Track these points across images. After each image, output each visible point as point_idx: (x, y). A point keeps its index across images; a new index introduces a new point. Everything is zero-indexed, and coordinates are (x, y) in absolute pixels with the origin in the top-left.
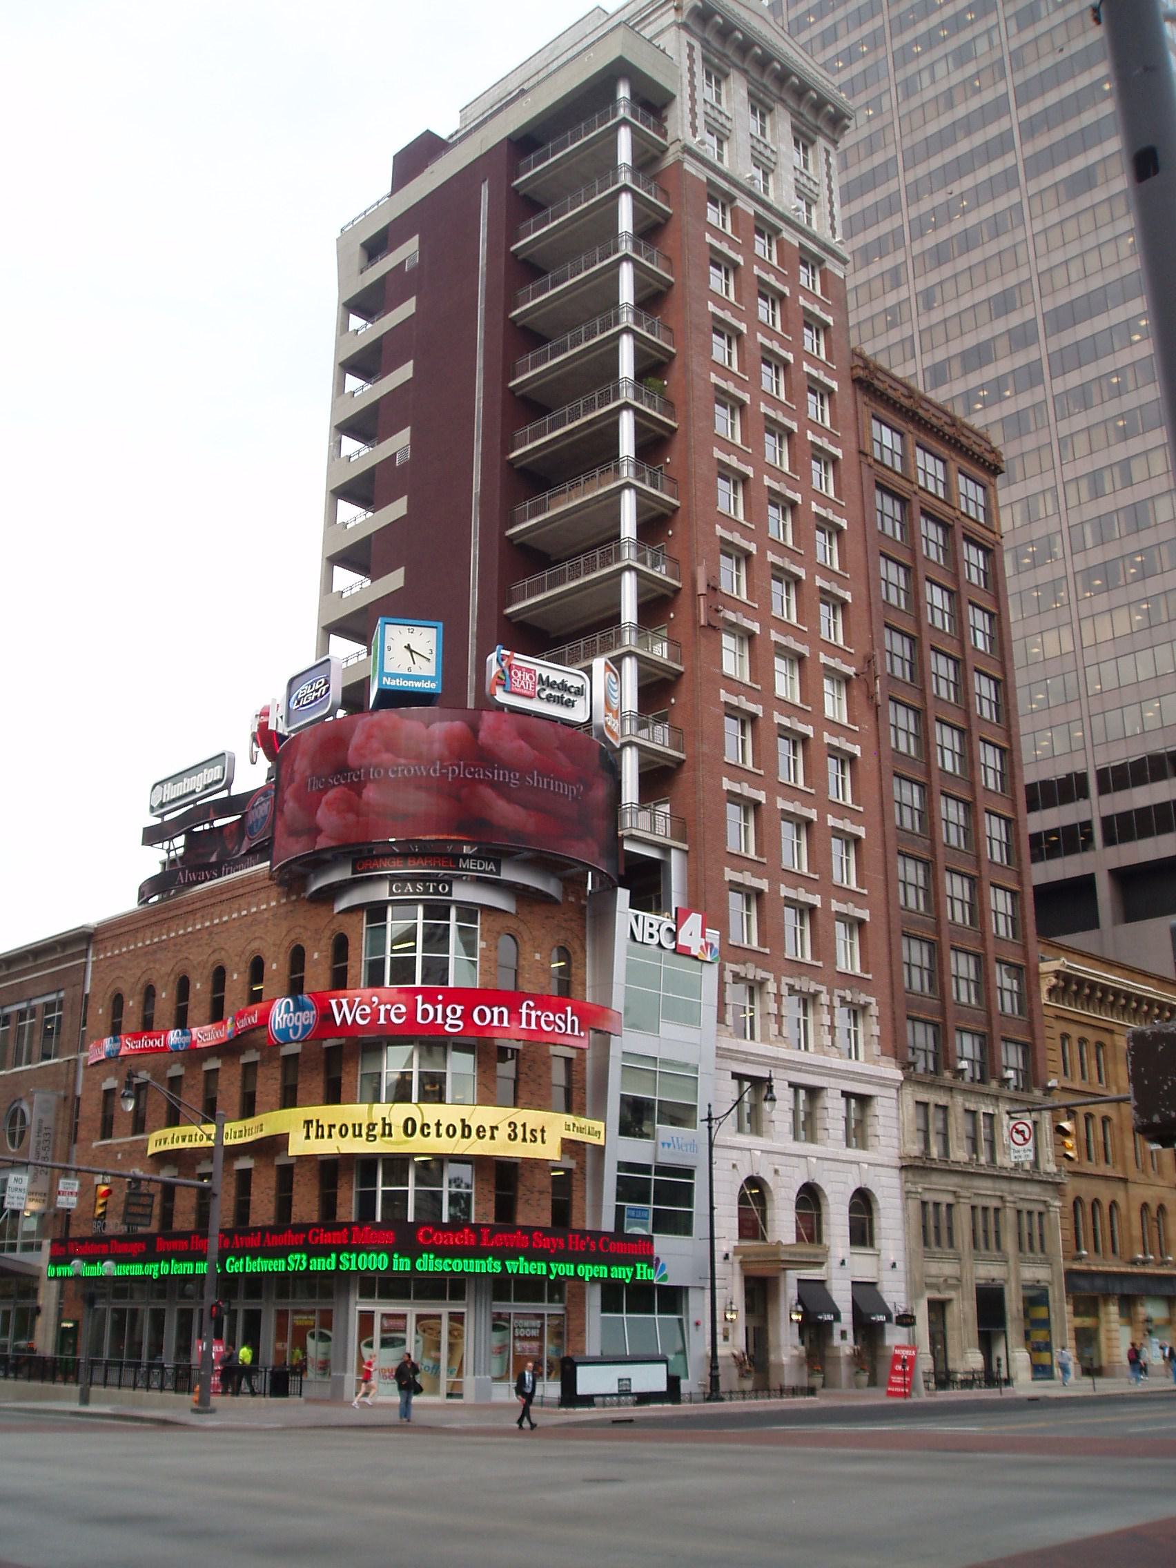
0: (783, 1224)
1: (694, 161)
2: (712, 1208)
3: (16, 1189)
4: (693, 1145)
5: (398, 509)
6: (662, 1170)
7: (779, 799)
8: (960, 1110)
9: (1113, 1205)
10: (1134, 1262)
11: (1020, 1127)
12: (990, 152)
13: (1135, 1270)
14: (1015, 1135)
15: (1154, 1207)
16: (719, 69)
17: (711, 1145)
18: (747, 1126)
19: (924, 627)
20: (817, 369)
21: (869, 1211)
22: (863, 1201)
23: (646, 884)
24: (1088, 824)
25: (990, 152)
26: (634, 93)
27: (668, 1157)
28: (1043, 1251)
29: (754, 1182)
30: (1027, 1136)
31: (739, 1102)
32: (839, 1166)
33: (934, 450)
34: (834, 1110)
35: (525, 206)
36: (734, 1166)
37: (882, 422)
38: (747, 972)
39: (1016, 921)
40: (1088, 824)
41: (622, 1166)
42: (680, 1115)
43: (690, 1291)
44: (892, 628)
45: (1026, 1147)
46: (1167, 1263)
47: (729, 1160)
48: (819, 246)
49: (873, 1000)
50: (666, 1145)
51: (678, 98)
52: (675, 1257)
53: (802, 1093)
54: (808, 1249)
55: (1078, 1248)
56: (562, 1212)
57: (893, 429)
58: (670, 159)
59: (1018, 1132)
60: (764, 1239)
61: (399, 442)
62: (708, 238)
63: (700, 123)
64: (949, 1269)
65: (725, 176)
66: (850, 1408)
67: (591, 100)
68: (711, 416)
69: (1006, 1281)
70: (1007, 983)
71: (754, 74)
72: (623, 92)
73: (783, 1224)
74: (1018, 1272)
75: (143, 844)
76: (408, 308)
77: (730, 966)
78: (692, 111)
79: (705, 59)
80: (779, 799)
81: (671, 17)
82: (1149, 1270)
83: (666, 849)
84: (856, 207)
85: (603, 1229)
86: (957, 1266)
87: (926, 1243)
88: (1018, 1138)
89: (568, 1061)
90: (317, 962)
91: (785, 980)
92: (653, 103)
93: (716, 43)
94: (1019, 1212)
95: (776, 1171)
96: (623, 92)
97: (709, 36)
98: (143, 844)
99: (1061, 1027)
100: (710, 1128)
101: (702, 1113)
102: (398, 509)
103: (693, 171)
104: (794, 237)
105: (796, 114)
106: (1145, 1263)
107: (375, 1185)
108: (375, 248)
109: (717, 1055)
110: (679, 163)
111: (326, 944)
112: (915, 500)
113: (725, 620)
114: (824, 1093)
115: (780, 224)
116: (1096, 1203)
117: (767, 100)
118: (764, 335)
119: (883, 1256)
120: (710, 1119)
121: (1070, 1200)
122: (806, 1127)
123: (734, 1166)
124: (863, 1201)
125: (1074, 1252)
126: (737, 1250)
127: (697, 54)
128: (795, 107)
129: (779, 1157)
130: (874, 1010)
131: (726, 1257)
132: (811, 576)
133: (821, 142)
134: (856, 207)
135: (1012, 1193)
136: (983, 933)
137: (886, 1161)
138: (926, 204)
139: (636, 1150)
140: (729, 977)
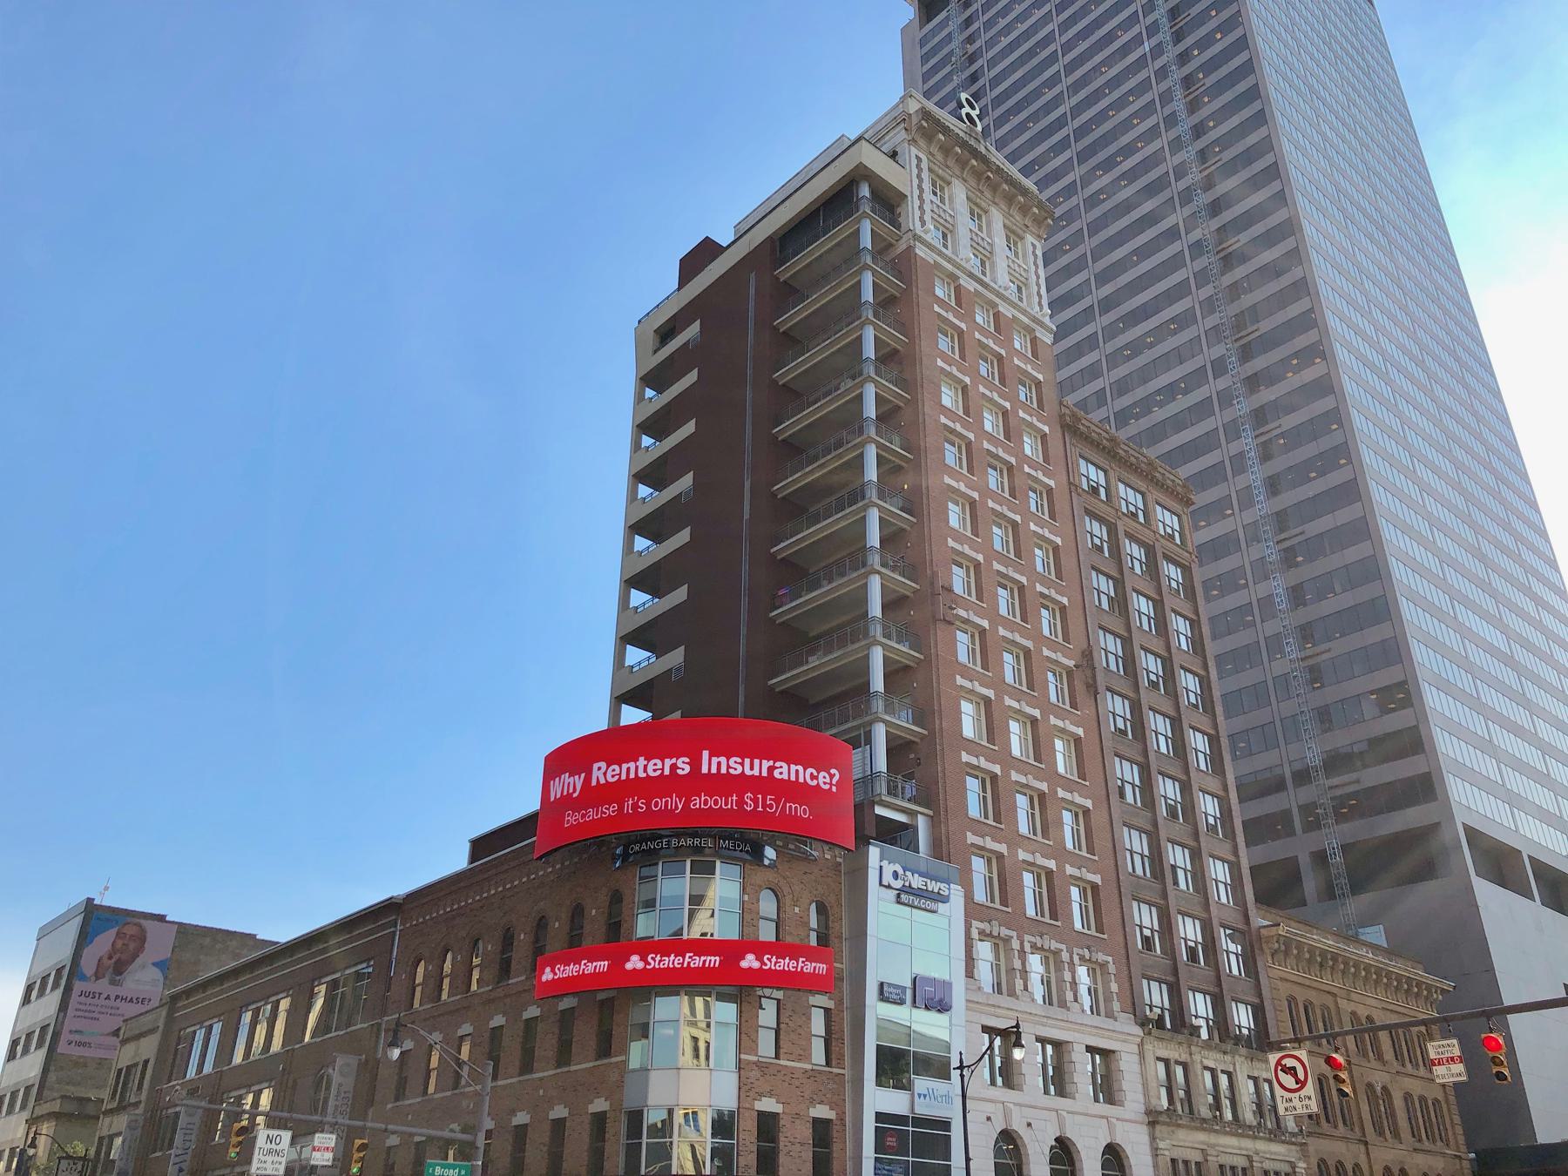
3: (270, 1152)
4: (948, 1098)
5: (680, 595)
6: (919, 1121)
8: (1199, 1067)
12: (1172, 296)
16: (942, 179)
17: (964, 1096)
18: (999, 1080)
19: (1134, 629)
23: (893, 834)
25: (1172, 296)
26: (872, 192)
27: (923, 1109)
31: (991, 1047)
34: (1083, 1068)
35: (789, 293)
36: (989, 1119)
38: (994, 917)
39: (1236, 885)
41: (880, 1117)
42: (937, 1067)
57: (1097, 467)
58: (902, 246)
63: (927, 217)
65: (949, 260)
67: (837, 202)
70: (1232, 947)
71: (972, 182)
72: (865, 191)
77: (975, 924)
78: (921, 208)
79: (930, 170)
81: (903, 134)
84: (1054, 267)
91: (1027, 938)
92: (888, 202)
93: (939, 156)
95: (1029, 1125)
96: (865, 191)
97: (934, 149)
100: (962, 1076)
101: (955, 1063)
102: (680, 595)
105: (1007, 215)
109: (968, 1009)
110: (910, 249)
112: (1119, 523)
115: (997, 300)
117: (983, 204)
120: (961, 1067)
121: (1314, 1161)
122: (1059, 1081)
123: (989, 1119)
127: (924, 165)
134: (1054, 267)
136: (1207, 899)
137: (1131, 1116)
138: (1121, 340)
140: (975, 934)
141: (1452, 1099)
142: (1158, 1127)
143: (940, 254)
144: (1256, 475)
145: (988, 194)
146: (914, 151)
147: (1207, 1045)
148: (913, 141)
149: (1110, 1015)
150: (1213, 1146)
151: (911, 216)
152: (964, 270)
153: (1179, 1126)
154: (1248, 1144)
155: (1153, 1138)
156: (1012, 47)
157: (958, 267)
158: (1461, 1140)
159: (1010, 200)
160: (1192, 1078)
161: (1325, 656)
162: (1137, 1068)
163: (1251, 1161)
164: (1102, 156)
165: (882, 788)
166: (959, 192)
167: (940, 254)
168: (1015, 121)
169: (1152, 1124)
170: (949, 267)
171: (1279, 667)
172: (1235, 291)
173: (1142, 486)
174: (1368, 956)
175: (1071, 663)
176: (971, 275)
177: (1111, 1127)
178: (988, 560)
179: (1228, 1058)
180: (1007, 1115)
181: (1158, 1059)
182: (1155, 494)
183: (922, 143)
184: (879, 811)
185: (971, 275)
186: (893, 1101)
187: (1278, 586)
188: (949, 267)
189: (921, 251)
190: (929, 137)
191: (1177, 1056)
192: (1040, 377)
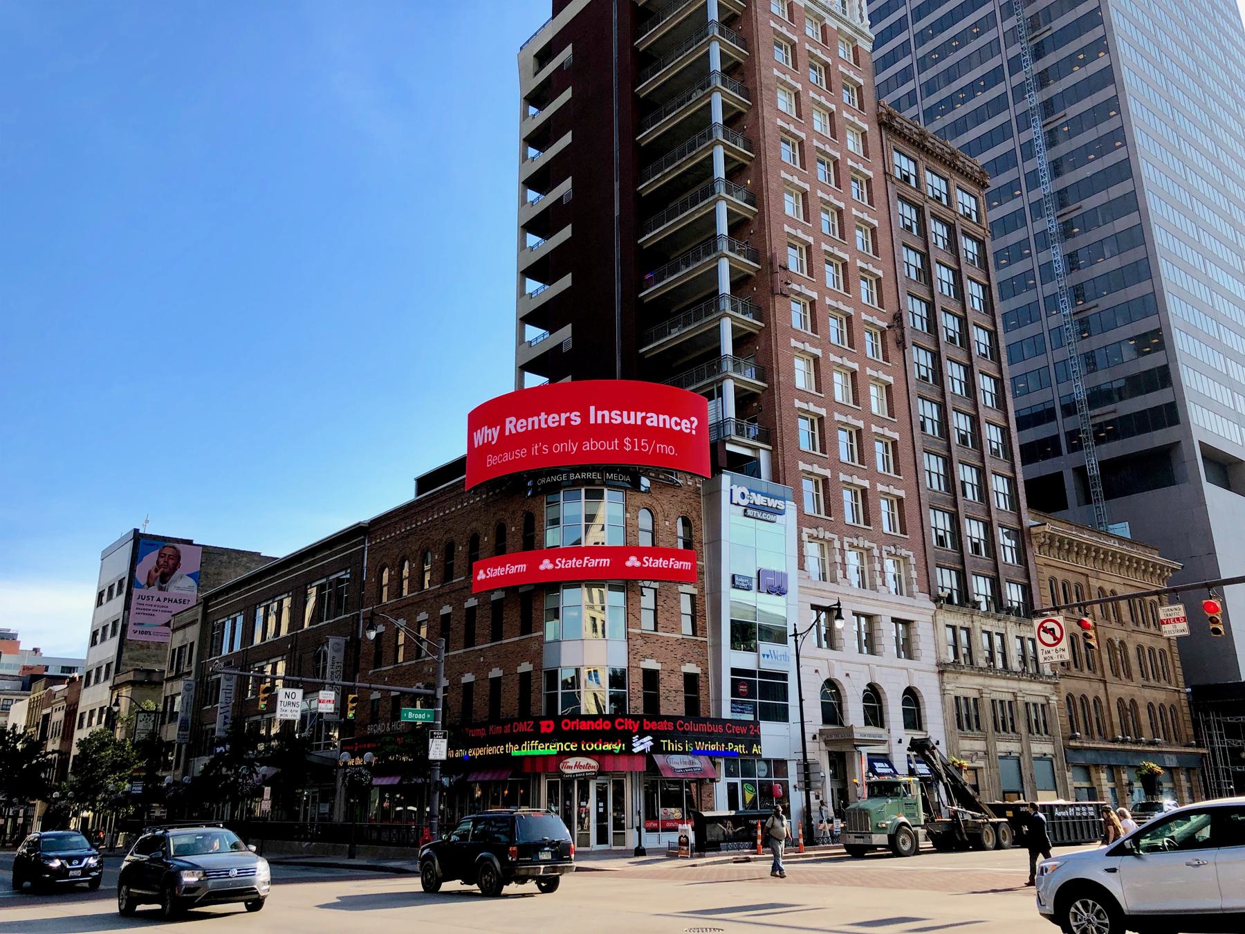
0: (854, 713)
2: (801, 700)
4: (785, 656)
6: (764, 674)
7: (836, 414)
9: (1097, 699)
10: (1115, 741)
11: (1049, 625)
13: (1117, 746)
14: (1042, 634)
15: (1127, 702)
21: (917, 704)
22: (911, 696)
24: (1057, 437)
27: (767, 665)
28: (978, 727)
29: (830, 683)
30: (1058, 634)
34: (888, 634)
40: (1057, 437)
41: (735, 671)
44: (913, 296)
45: (1058, 647)
46: (1141, 742)
47: (807, 669)
49: (911, 553)
50: (770, 657)
52: (776, 739)
53: (863, 620)
54: (873, 731)
55: (1073, 731)
56: (692, 704)
57: (909, 158)
59: (1046, 631)
60: (842, 724)
61: (565, 187)
62: (772, 24)
68: (778, 149)
70: (1008, 542)
73: (854, 713)
76: (567, 95)
77: (805, 530)
80: (836, 414)
82: (1128, 747)
83: (755, 449)
86: (983, 743)
87: (960, 726)
88: (1048, 638)
89: (692, 596)
90: (514, 534)
91: (846, 539)
94: (1027, 704)
99: (1048, 573)
101: (790, 631)
106: (1124, 741)
107: (556, 689)
108: (543, 57)
111: (520, 518)
112: (926, 206)
113: (792, 290)
114: (879, 619)
116: (1084, 698)
118: (814, 91)
120: (796, 635)
124: (911, 696)
125: (1070, 734)
126: (821, 732)
129: (854, 671)
130: (912, 560)
131: (814, 738)
132: (862, 366)
139: (745, 660)
142: (946, 675)
144: (1042, 161)
154: (1014, 685)
155: (942, 682)
158: (1181, 679)
160: (972, 638)
162: (931, 633)
165: (731, 430)
169: (941, 673)
175: (884, 325)
179: (1002, 624)
184: (729, 447)
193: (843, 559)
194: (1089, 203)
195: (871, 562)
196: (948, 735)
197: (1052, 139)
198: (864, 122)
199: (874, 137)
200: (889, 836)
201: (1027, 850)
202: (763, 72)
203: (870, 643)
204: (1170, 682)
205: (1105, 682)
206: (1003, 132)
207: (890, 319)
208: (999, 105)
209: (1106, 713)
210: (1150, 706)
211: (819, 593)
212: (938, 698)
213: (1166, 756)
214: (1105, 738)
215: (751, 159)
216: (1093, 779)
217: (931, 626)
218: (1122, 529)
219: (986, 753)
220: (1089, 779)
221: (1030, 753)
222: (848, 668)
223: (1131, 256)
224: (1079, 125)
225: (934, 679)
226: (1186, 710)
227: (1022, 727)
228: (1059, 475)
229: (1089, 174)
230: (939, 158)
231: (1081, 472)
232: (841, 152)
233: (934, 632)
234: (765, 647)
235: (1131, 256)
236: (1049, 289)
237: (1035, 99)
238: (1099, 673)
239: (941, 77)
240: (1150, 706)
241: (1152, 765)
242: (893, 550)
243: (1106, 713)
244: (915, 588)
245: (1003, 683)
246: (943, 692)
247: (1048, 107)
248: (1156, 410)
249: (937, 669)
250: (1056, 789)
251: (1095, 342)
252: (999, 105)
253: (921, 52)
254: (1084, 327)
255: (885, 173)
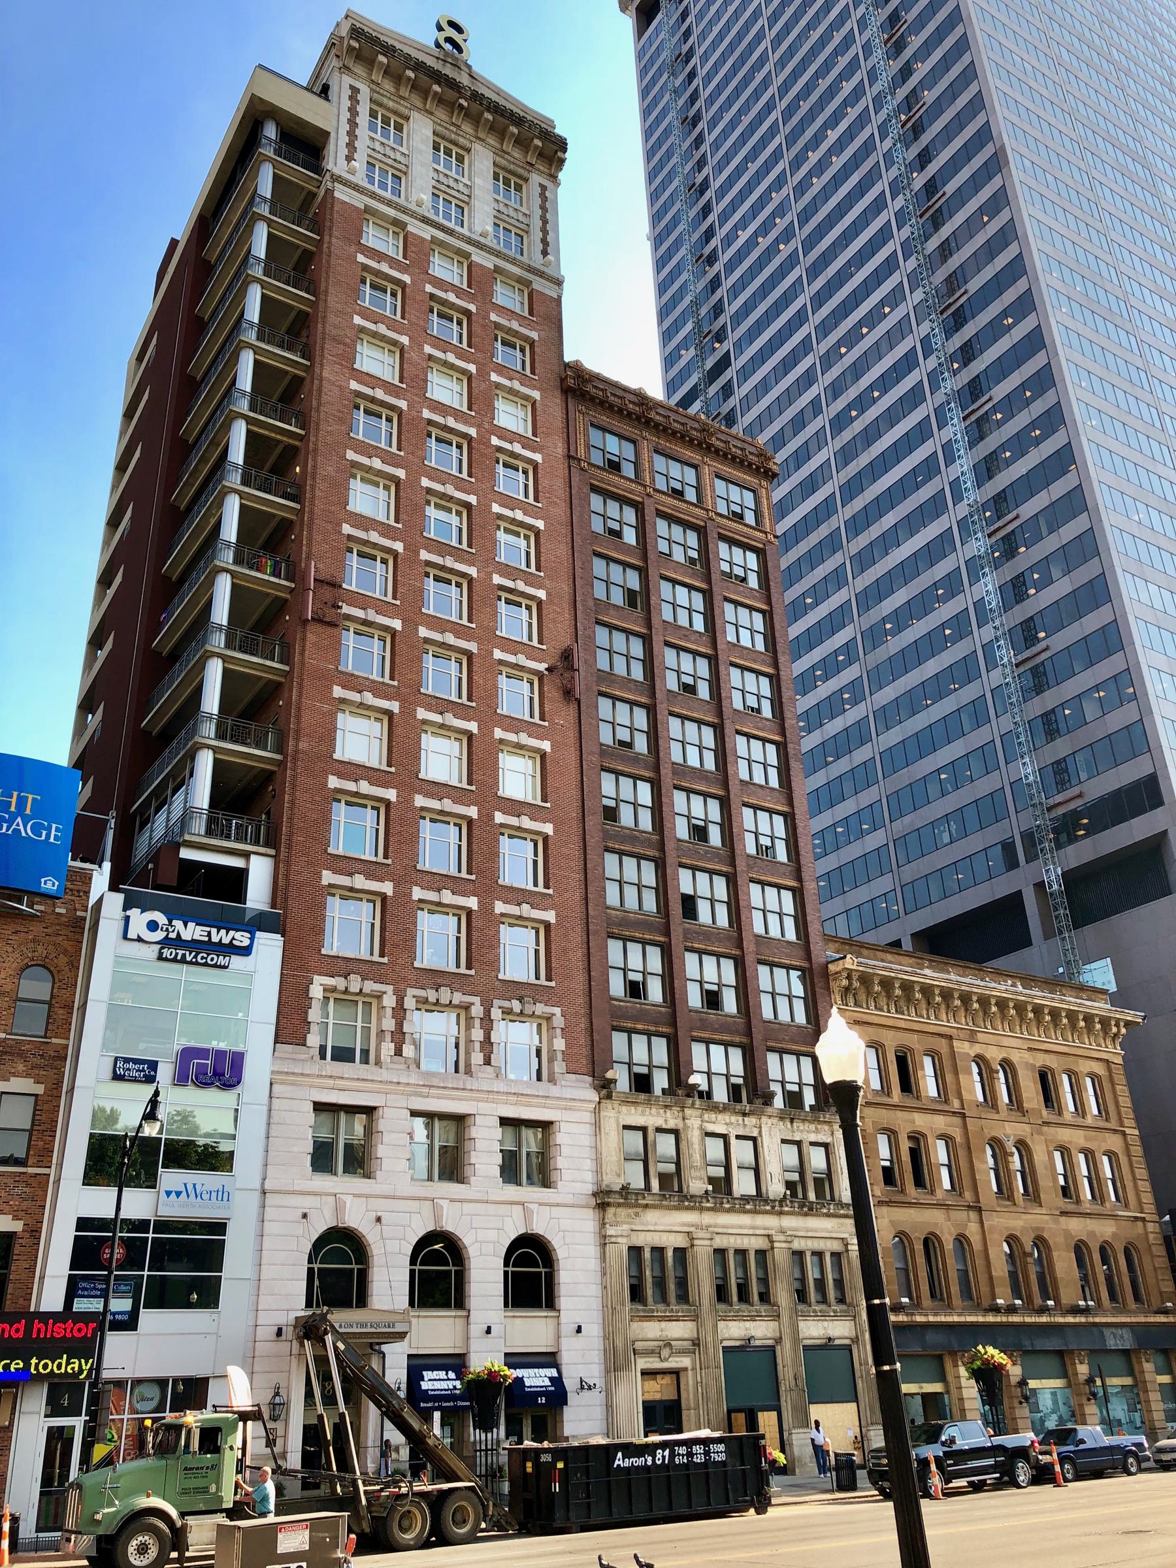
1: (346, 189)
6: (162, 1225)
9: (961, 1241)
10: (996, 1309)
20: (511, 379)
32: (492, 1208)
33: (678, 456)
36: (305, 1216)
37: (604, 430)
43: (211, 1381)
48: (522, 268)
49: (557, 1011)
51: (333, 135)
57: (621, 437)
64: (680, 1330)
66: (607, 490)
69: (779, 1340)
72: (270, 131)
74: (795, 1330)
75: (85, 1183)
82: (1015, 1319)
85: (44, 1308)
86: (690, 1325)
91: (411, 992)
93: (388, 85)
96: (270, 131)
97: (377, 76)
98: (85, 1183)
103: (346, 199)
104: (488, 260)
106: (1011, 1309)
110: (329, 192)
112: (647, 501)
114: (470, 1121)
116: (930, 1243)
117: (461, 141)
119: (563, 1319)
128: (498, 146)
130: (559, 1021)
133: (536, 179)
135: (783, 1232)
141: (1137, 1150)
142: (611, 1211)
143: (373, 196)
144: (964, 465)
145: (467, 128)
146: (347, 80)
147: (724, 1109)
148: (345, 69)
149: (552, 1080)
150: (699, 1227)
151: (335, 160)
152: (413, 215)
153: (646, 1206)
154: (769, 1222)
155: (603, 1224)
156: (721, 36)
157: (404, 210)
158: (1148, 1198)
159: (502, 134)
160: (683, 1145)
161: (1044, 656)
162: (587, 1141)
163: (772, 1242)
164: (809, 133)
165: (199, 826)
166: (421, 129)
167: (373, 196)
168: (727, 117)
169: (602, 1206)
170: (391, 212)
171: (996, 677)
172: (945, 251)
173: (696, 457)
174: (1100, 1007)
175: (542, 667)
176: (425, 220)
177: (527, 1215)
178: (412, 549)
179: (751, 1121)
180: (339, 1208)
181: (415, 1114)
182: (710, 466)
183: (359, 70)
184: (186, 854)
185: (425, 220)
186: (100, 1202)
187: (988, 586)
188: (391, 212)
189: (342, 194)
190: (369, 63)
191: (660, 1122)
192: (534, 335)
193: (399, 1025)
194: (1028, 509)
195: (469, 1028)
196: (609, 1312)
197: (979, 430)
198: (534, 388)
199: (554, 407)
200: (100, 1539)
201: (891, 1504)
202: (332, 319)
203: (451, 1165)
204: (1126, 1206)
205: (979, 1210)
206: (922, 432)
207: (554, 660)
208: (914, 397)
209: (980, 1262)
210: (1080, 1250)
211: (331, 1082)
212: (593, 1251)
213: (1107, 1332)
214: (978, 1308)
215: (301, 438)
216: (950, 1378)
217: (588, 1129)
218: (1101, 973)
219: (696, 1343)
220: (942, 1378)
221: (796, 1339)
222: (381, 1206)
223: (1085, 573)
224: (1011, 405)
225: (587, 1221)
226: (1160, 1251)
227: (783, 1294)
228: (1018, 894)
229: (1024, 471)
230: (682, 438)
231: (1040, 886)
232: (479, 427)
233: (590, 1138)
234: (170, 1178)
235: (1085, 573)
236: (988, 633)
237: (952, 384)
238: (968, 1195)
239: (848, 374)
240: (1080, 1250)
241: (991, 1350)
242: (516, 1006)
243: (980, 1262)
244: (559, 1066)
245: (745, 1220)
246: (604, 1241)
247: (975, 389)
248: (1136, 786)
249: (593, 1202)
250: (856, 1400)
251: (1049, 699)
252: (914, 397)
253: (824, 347)
254: (1038, 679)
255: (569, 457)
